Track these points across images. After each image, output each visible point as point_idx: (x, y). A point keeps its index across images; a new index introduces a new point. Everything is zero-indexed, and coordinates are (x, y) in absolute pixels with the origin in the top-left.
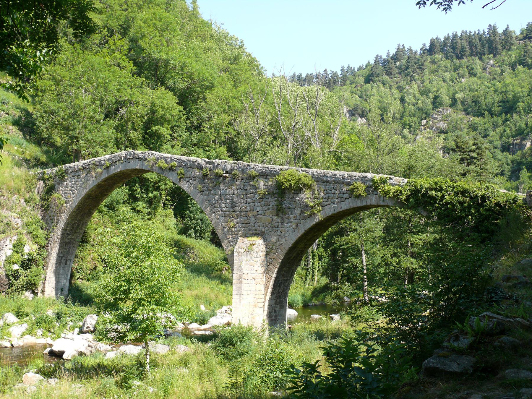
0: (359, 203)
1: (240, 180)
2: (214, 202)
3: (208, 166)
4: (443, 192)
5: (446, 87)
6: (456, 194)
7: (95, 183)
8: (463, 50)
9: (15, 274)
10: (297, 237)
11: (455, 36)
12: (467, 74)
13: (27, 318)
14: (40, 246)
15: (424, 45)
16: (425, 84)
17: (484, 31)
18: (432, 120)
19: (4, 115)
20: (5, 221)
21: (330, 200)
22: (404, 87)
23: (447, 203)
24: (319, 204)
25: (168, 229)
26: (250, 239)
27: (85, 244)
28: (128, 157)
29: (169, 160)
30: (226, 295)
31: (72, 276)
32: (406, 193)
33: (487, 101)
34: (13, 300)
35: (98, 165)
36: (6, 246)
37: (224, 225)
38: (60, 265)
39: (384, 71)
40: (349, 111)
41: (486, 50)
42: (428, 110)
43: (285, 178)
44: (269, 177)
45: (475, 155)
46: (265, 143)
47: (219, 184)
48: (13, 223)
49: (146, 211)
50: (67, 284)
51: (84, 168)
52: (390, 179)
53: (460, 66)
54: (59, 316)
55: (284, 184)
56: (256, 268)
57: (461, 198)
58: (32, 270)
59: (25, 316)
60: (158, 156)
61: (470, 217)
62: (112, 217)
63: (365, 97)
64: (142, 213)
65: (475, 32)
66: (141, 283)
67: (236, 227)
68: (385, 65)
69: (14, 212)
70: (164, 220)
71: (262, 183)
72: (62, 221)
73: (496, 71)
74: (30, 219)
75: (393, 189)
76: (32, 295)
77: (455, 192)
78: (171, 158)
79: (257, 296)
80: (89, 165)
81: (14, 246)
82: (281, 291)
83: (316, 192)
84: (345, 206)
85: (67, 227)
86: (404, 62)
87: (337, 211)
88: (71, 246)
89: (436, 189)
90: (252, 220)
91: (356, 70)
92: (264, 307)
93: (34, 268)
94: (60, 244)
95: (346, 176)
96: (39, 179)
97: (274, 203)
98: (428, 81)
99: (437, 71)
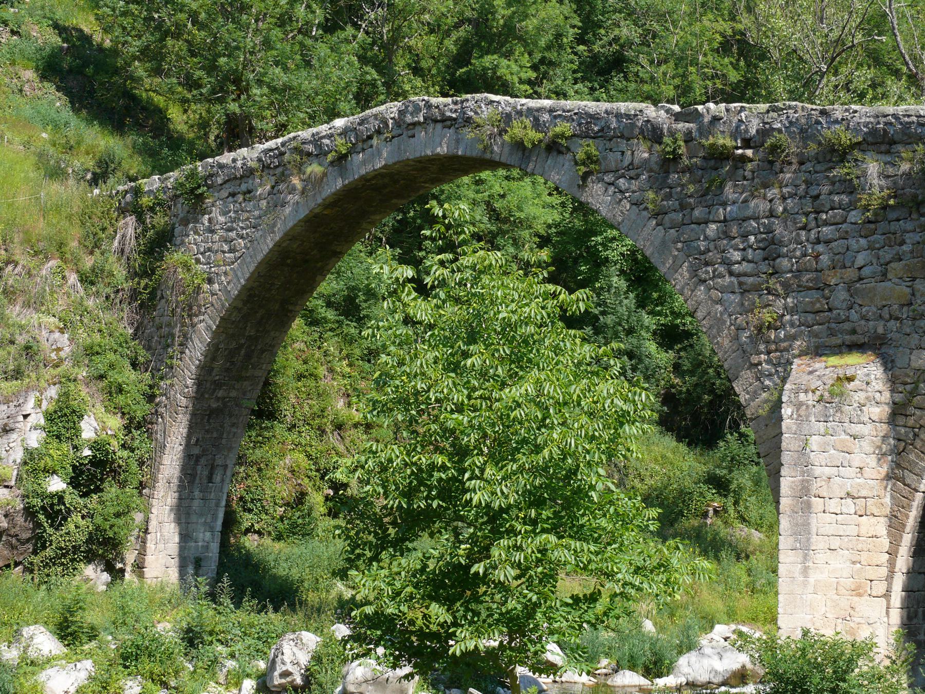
1: (794, 167)
2: (702, 245)
3: (681, 126)
7: (303, 213)
9: (52, 505)
13: (93, 644)
14: (131, 420)
19: (6, 37)
20: (21, 340)
26: (833, 360)
27: (267, 423)
28: (409, 119)
29: (546, 117)
30: (721, 588)
31: (230, 521)
34: (49, 590)
35: (309, 154)
36: (25, 416)
37: (741, 319)
38: (191, 482)
44: (900, 148)
47: (721, 187)
48: (45, 346)
50: (215, 547)
51: (266, 167)
56: (857, 459)
58: (106, 496)
59: (84, 639)
60: (508, 109)
62: (349, 340)
66: (497, 459)
67: (783, 326)
71: (873, 168)
72: (196, 341)
74: (97, 337)
76: (106, 577)
78: (551, 111)
79: (864, 557)
81: (50, 417)
85: (214, 359)
90: (841, 295)
92: (887, 595)
93: (111, 490)
94: (193, 415)
96: (123, 211)
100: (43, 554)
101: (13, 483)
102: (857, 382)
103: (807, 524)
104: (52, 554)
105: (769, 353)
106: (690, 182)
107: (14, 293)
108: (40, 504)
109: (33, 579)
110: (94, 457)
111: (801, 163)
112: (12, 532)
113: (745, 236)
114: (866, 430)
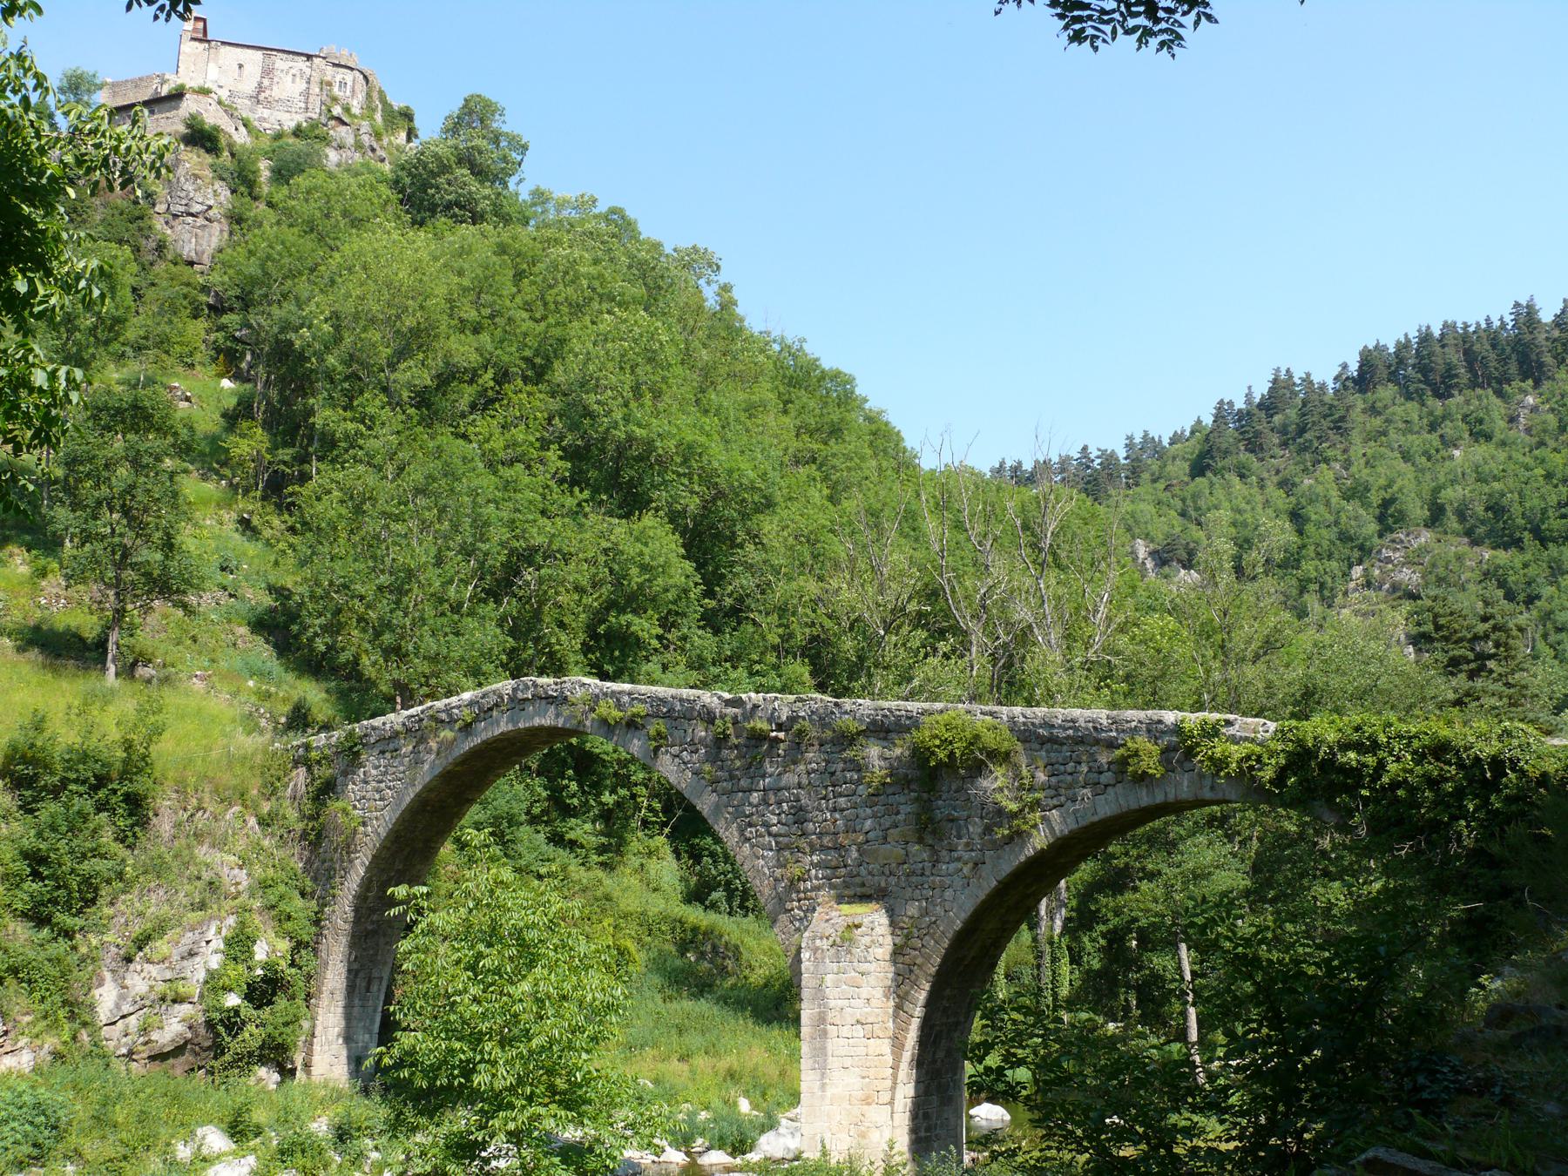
0: (1143, 798)
3: (730, 711)
4: (1381, 754)
5: (1411, 476)
6: (1419, 757)
7: (437, 771)
8: (1449, 373)
9: (229, 1018)
10: (979, 901)
11: (1425, 338)
12: (1466, 436)
13: (258, 1140)
15: (1345, 366)
16: (1354, 469)
17: (1501, 319)
18: (1378, 564)
20: (206, 876)
21: (1063, 791)
22: (1297, 480)
23: (1395, 785)
24: (1036, 804)
25: (655, 890)
26: (845, 908)
28: (520, 695)
29: (626, 699)
32: (1273, 761)
33: (1528, 505)
35: (442, 721)
36: (208, 942)
37: (778, 872)
39: (1240, 441)
40: (1153, 554)
41: (1513, 368)
42: (1365, 539)
43: (936, 737)
45: (1489, 647)
46: (904, 645)
47: (761, 762)
48: (226, 880)
49: (594, 840)
51: (409, 730)
52: (1229, 723)
53: (1444, 418)
54: (342, 1135)
55: (933, 753)
56: (865, 992)
57: (1432, 767)
58: (277, 1008)
59: (251, 1136)
60: (597, 691)
61: (1463, 823)
63: (1193, 514)
64: (582, 847)
65: (1478, 324)
68: (1243, 426)
69: (229, 852)
70: (642, 865)
73: (1544, 422)
74: (271, 872)
75: (1237, 752)
76: (276, 1077)
77: (1415, 752)
78: (630, 694)
79: (872, 1072)
80: (421, 720)
81: (229, 943)
82: (941, 1054)
83: (1025, 772)
84: (1106, 807)
86: (1292, 414)
87: (1083, 823)
88: (382, 941)
89: (1358, 747)
91: (1166, 442)
92: (891, 1103)
93: (281, 1002)
95: (1105, 722)
96: (296, 763)
97: (908, 809)
98: (1363, 461)
99: (1385, 434)
100: (222, 1059)
101: (196, 1000)
102: (863, 929)
103: (824, 1048)
104: (230, 1059)
105: (799, 900)
106: (737, 757)
107: (202, 835)
108: (219, 1017)
109: (213, 1082)
110: (265, 975)
111: (821, 745)
112: (195, 1041)
113: (779, 803)
114: (871, 967)
